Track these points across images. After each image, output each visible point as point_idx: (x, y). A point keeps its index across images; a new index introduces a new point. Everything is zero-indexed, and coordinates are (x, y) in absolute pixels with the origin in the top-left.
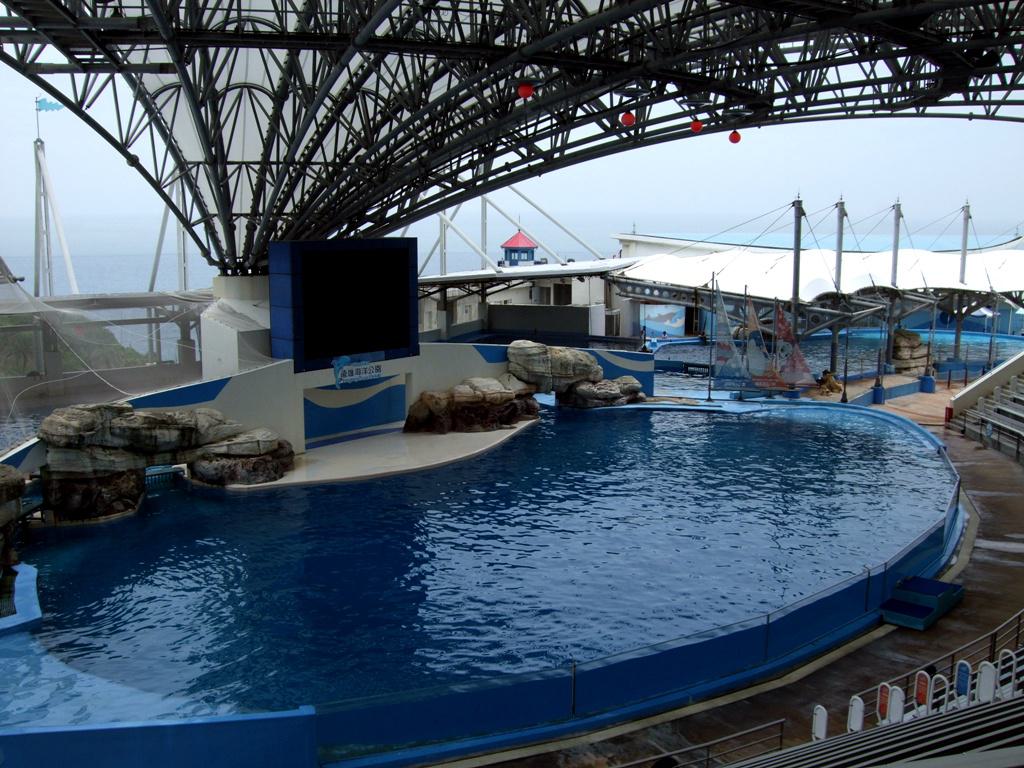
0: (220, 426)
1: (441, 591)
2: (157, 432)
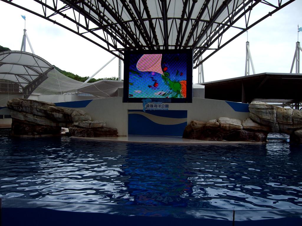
0: (81, 116)
2: (54, 113)
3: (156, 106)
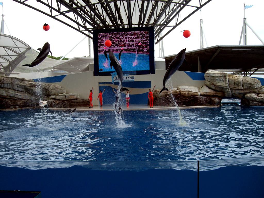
0: (57, 90)
1: (36, 160)
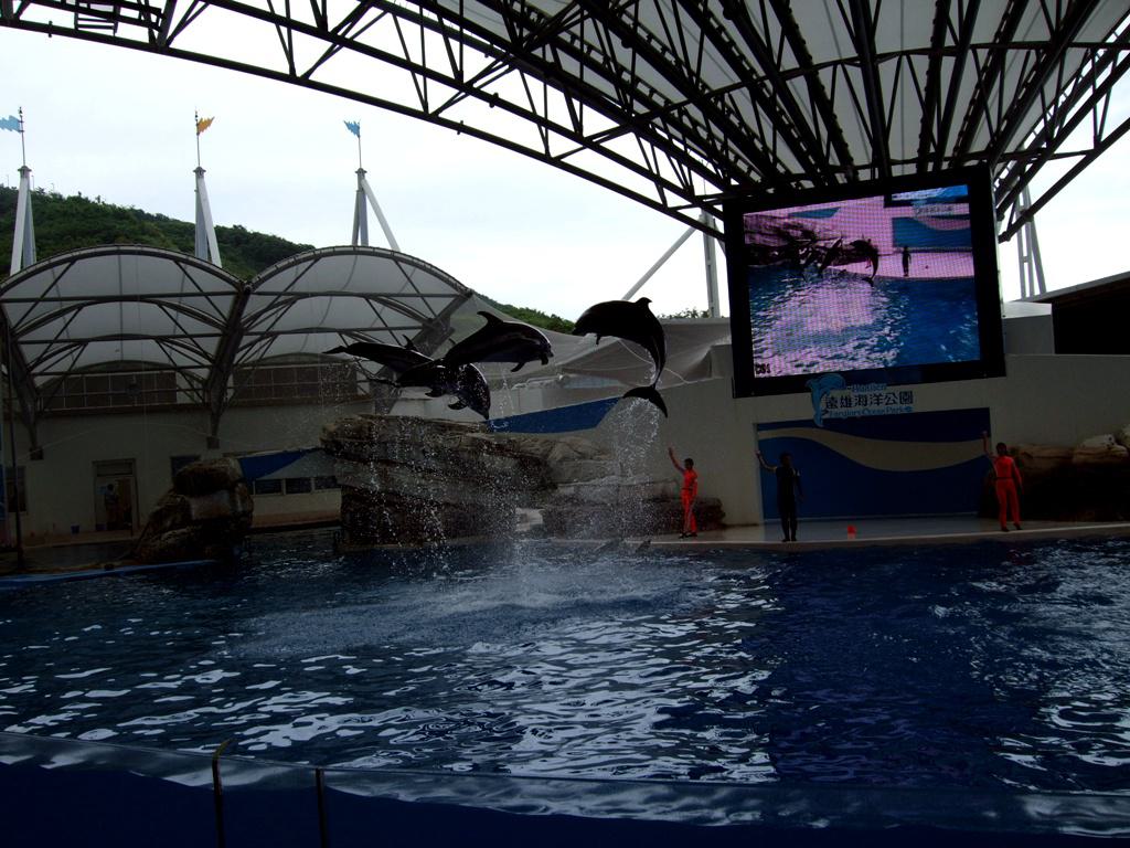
3: (862, 400)
